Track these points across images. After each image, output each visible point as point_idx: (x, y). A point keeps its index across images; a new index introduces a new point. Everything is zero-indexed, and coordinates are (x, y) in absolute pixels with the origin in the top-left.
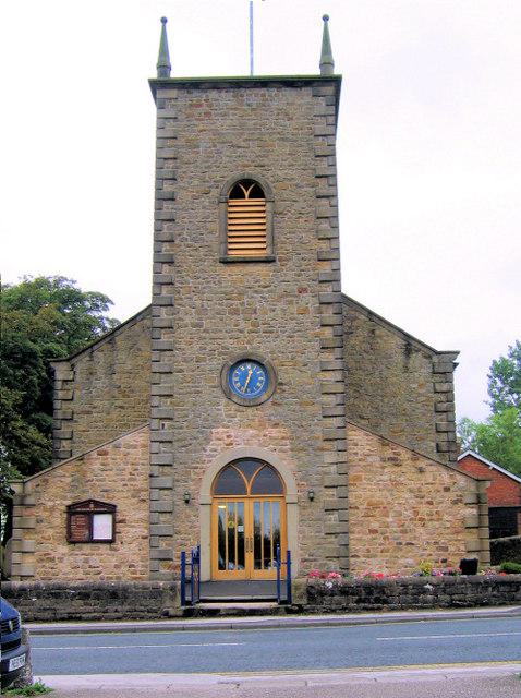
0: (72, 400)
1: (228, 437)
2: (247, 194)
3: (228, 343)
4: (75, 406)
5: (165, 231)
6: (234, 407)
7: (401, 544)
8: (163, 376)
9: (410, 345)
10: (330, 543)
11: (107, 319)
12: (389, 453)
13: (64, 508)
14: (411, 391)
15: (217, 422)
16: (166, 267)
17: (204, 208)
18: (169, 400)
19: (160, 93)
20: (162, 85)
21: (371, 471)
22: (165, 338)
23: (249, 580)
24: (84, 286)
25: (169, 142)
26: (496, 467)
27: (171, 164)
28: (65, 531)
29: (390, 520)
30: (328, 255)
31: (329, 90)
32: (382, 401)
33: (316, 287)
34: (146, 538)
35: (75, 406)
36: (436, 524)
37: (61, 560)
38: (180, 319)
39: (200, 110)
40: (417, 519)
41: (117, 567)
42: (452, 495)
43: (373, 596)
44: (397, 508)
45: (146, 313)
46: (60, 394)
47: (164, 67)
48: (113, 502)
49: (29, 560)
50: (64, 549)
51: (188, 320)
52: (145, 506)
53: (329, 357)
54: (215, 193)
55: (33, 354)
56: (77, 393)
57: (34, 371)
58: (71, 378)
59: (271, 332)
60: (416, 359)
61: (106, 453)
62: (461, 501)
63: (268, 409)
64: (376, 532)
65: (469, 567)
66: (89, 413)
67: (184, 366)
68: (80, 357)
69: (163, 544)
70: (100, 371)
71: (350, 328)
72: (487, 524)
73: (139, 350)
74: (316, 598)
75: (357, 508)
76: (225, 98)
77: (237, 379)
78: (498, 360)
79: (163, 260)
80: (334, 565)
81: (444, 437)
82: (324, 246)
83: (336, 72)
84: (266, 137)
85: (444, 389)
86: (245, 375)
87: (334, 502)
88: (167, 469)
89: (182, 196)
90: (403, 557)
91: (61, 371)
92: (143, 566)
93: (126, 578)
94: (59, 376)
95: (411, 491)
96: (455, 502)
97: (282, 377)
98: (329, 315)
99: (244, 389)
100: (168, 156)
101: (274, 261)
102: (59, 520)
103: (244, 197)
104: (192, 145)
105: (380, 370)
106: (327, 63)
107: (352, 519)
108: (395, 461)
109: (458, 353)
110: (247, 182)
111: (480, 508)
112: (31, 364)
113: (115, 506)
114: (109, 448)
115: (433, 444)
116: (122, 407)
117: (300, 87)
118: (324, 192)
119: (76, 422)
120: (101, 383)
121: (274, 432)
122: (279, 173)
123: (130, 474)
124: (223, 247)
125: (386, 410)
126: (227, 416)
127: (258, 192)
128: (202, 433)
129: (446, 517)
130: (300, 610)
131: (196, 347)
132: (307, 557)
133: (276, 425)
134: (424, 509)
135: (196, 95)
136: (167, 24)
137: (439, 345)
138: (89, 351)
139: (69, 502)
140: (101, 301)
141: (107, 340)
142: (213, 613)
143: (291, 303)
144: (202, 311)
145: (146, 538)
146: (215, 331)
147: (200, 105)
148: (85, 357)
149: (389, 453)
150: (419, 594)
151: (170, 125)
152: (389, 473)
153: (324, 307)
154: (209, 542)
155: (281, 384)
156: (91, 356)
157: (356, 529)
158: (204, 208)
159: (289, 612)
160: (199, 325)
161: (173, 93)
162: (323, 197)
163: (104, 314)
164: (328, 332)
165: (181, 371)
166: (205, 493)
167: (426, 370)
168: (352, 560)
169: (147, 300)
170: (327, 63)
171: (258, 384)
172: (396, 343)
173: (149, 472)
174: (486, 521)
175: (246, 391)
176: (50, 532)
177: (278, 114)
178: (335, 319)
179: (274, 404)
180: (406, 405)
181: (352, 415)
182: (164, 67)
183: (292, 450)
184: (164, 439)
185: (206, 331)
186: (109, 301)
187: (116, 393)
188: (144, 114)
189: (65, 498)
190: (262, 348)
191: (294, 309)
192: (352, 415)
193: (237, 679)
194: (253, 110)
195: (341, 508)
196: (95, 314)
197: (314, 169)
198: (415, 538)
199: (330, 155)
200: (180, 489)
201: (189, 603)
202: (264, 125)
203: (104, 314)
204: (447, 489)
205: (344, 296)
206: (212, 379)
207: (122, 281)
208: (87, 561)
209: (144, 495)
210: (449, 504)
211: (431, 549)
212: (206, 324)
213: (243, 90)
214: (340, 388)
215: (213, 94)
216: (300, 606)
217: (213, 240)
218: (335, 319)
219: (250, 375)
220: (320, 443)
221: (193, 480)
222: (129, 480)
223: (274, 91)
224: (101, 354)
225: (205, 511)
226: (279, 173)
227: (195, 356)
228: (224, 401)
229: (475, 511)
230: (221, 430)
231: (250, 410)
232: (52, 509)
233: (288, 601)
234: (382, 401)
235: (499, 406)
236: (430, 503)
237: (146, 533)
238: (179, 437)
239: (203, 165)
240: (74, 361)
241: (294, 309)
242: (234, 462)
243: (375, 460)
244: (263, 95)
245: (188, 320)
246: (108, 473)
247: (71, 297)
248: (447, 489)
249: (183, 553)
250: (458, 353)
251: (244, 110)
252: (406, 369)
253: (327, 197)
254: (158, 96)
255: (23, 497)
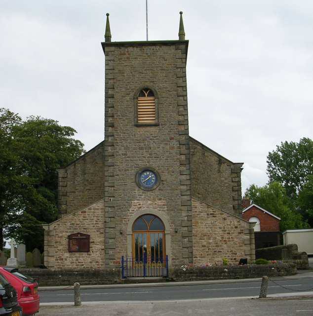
0: (66, 186)
1: (139, 204)
2: (146, 95)
3: (140, 163)
4: (68, 189)
5: (110, 112)
6: (141, 191)
7: (216, 251)
8: (110, 177)
9: (221, 160)
10: (186, 251)
11: (74, 140)
12: (211, 211)
13: (66, 236)
14: (222, 181)
15: (134, 198)
16: (110, 128)
17: (127, 101)
18: (113, 188)
19: (107, 49)
20: (107, 45)
21: (203, 219)
22: (110, 160)
23: (154, 266)
24: (62, 124)
25: (111, 71)
26: (266, 211)
27: (112, 81)
28: (67, 246)
29: (211, 241)
30: (184, 123)
31: (183, 47)
32: (208, 186)
33: (178, 137)
34: (103, 249)
35: (68, 189)
36: (232, 243)
37: (66, 259)
38: (117, 152)
39: (125, 56)
40: (222, 237)
41: (90, 262)
42: (239, 230)
43: (203, 274)
44: (214, 236)
45: (102, 145)
46: (61, 184)
47: (108, 36)
48: (89, 234)
49: (52, 260)
50: (67, 255)
51: (120, 152)
52: (103, 235)
53: (183, 168)
54: (132, 94)
55: (39, 159)
56: (69, 183)
57: (40, 168)
58: (66, 176)
59: (158, 157)
60: (224, 167)
61: (85, 212)
62: (242, 233)
63: (157, 192)
64: (205, 246)
65: (243, 261)
66: (75, 192)
67: (119, 173)
68: (69, 167)
69: (111, 252)
70: (79, 173)
71: (193, 152)
72: (254, 243)
73: (97, 163)
74: (179, 275)
75: (196, 236)
76: (136, 50)
77: (143, 176)
78: (272, 153)
79: (108, 125)
80: (186, 261)
81: (236, 202)
82: (181, 118)
83: (186, 39)
84: (155, 69)
85: (237, 180)
86: (147, 176)
87: (186, 233)
88: (112, 219)
89: (117, 96)
90: (216, 257)
91: (61, 173)
92: (102, 262)
93: (95, 266)
94: (60, 175)
95: (220, 228)
96: (240, 233)
97: (163, 178)
98: (183, 149)
99: (144, 181)
100: (110, 78)
101: (159, 125)
102: (65, 242)
103: (145, 96)
104: (121, 72)
105: (210, 172)
106: (182, 33)
107: (194, 241)
108: (213, 215)
109: (243, 163)
110: (146, 90)
111: (250, 235)
112: (38, 164)
113: (89, 236)
114: (86, 209)
115: (232, 206)
116: (89, 190)
117: (170, 46)
118: (181, 94)
119: (68, 196)
120: (79, 179)
121: (159, 203)
122: (161, 85)
123: (96, 221)
124: (136, 120)
125: (210, 190)
126: (138, 195)
127: (151, 94)
128: (127, 203)
129: (235, 240)
130: (173, 280)
131: (124, 165)
132: (174, 258)
133: (160, 199)
134: (226, 236)
135: (123, 49)
136: (109, 17)
137: (234, 160)
138: (74, 163)
139: (70, 234)
140: (82, 145)
141: (82, 158)
142: (134, 282)
143: (166, 144)
144: (127, 148)
145: (103, 249)
146: (133, 157)
147: (125, 54)
148: (72, 167)
149: (211, 211)
150: (222, 273)
151: (111, 63)
152: (210, 220)
153: (181, 146)
154: (131, 251)
155: (162, 181)
156: (75, 166)
157: (195, 245)
158: (127, 101)
159: (168, 281)
160: (125, 155)
161: (113, 49)
162: (181, 96)
163: (72, 137)
164: (183, 157)
165: (118, 175)
166: (129, 229)
167: (229, 172)
168: (194, 259)
169: (102, 138)
170: (182, 33)
171: (153, 181)
172: (214, 159)
173: (104, 221)
174: (254, 241)
175: (144, 182)
176: (61, 247)
177: (160, 58)
178: (186, 152)
179: (159, 190)
180: (219, 188)
181: (193, 193)
182: (108, 36)
183: (167, 210)
184: (111, 205)
185: (128, 157)
186: (75, 131)
187: (86, 183)
188: (99, 59)
189: (67, 232)
190: (154, 164)
191: (168, 147)
192: (193, 193)
193: (152, 302)
194: (149, 56)
195: (189, 235)
196: (67, 137)
197: (177, 83)
198: (222, 249)
199: (184, 76)
200: (118, 228)
201: (125, 277)
202: (153, 63)
203: (72, 137)
204: (236, 227)
205: (190, 137)
206: (132, 179)
207: (90, 134)
208: (77, 260)
209: (102, 231)
210: (237, 234)
211: (229, 254)
212: (129, 154)
213: (144, 47)
214: (188, 182)
215: (131, 49)
216: (172, 278)
217: (131, 115)
218: (186, 152)
219: (148, 177)
220: (180, 207)
221: (124, 224)
222: (96, 224)
223: (158, 47)
224: (79, 165)
225: (129, 238)
226: (161, 85)
227: (123, 166)
228: (137, 188)
229: (248, 237)
230: (136, 201)
231: (149, 193)
232: (61, 237)
233: (167, 276)
234: (208, 186)
235: (274, 177)
236: (229, 233)
237: (103, 247)
238: (117, 205)
239: (127, 82)
240: (67, 168)
241: (168, 147)
242: (142, 216)
243: (203, 215)
244: (153, 49)
245: (120, 152)
246: (86, 221)
247: (58, 129)
248: (236, 227)
249: (123, 257)
250: (243, 163)
251: (145, 56)
252: (219, 171)
253: (183, 96)
254: (106, 50)
255: (49, 232)
